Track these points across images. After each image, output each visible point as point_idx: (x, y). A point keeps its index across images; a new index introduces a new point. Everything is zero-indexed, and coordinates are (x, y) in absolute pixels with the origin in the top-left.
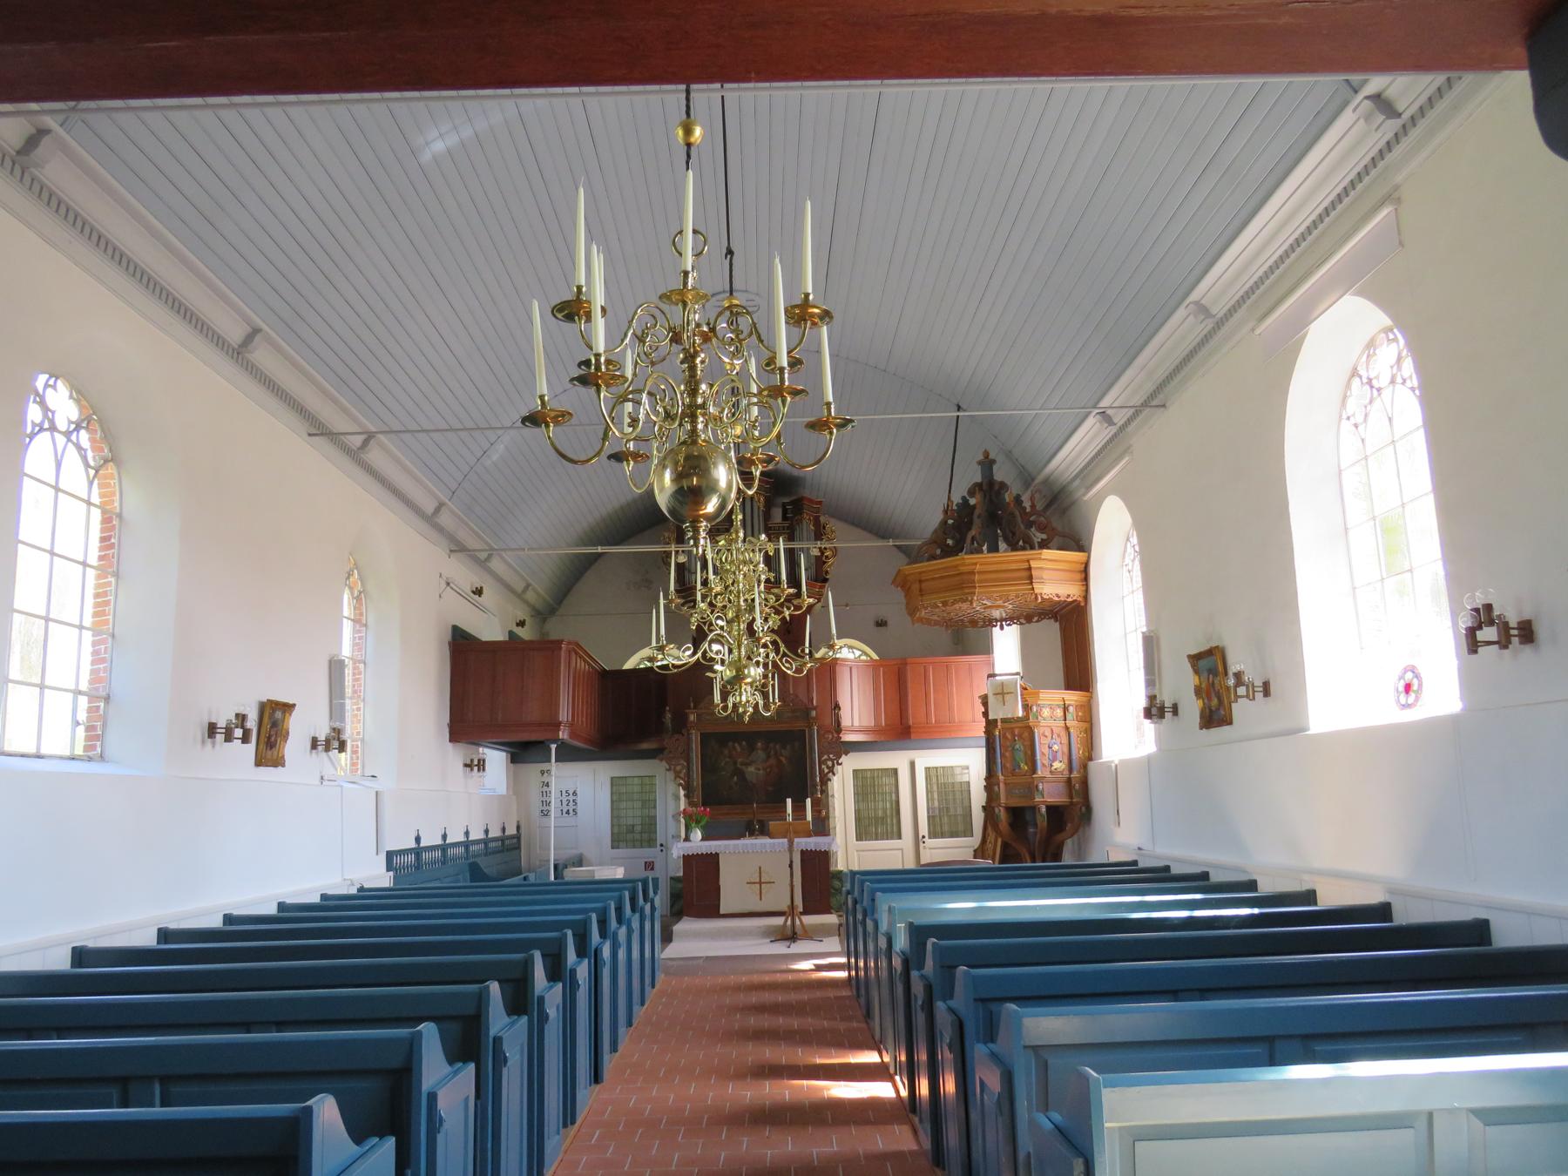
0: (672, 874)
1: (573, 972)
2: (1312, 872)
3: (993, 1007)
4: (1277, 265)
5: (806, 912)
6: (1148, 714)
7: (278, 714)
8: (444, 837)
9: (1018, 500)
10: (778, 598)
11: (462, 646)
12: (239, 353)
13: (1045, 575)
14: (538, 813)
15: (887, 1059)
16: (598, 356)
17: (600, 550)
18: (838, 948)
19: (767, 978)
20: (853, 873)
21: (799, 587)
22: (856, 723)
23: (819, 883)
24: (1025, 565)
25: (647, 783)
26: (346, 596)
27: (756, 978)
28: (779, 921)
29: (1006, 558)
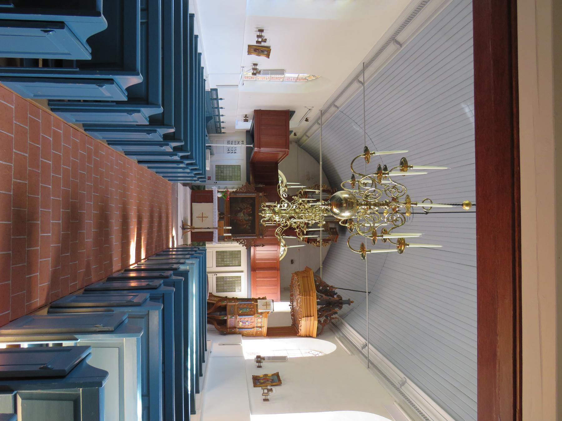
0: (206, 186)
1: (176, 155)
2: (202, 413)
3: (161, 300)
4: (419, 411)
5: (192, 233)
6: (258, 357)
7: (266, 53)
8: (222, 108)
9: (336, 313)
10: (303, 227)
11: (288, 114)
12: (393, 39)
13: (308, 322)
14: (229, 140)
15: (143, 261)
16: (388, 174)
17: (321, 163)
18: (179, 244)
19: (170, 219)
20: (205, 250)
21: (307, 235)
22: (257, 252)
23: (202, 238)
24: (312, 315)
25: (238, 178)
26: (306, 75)
27: (170, 216)
28: (189, 224)
29: (315, 308)
